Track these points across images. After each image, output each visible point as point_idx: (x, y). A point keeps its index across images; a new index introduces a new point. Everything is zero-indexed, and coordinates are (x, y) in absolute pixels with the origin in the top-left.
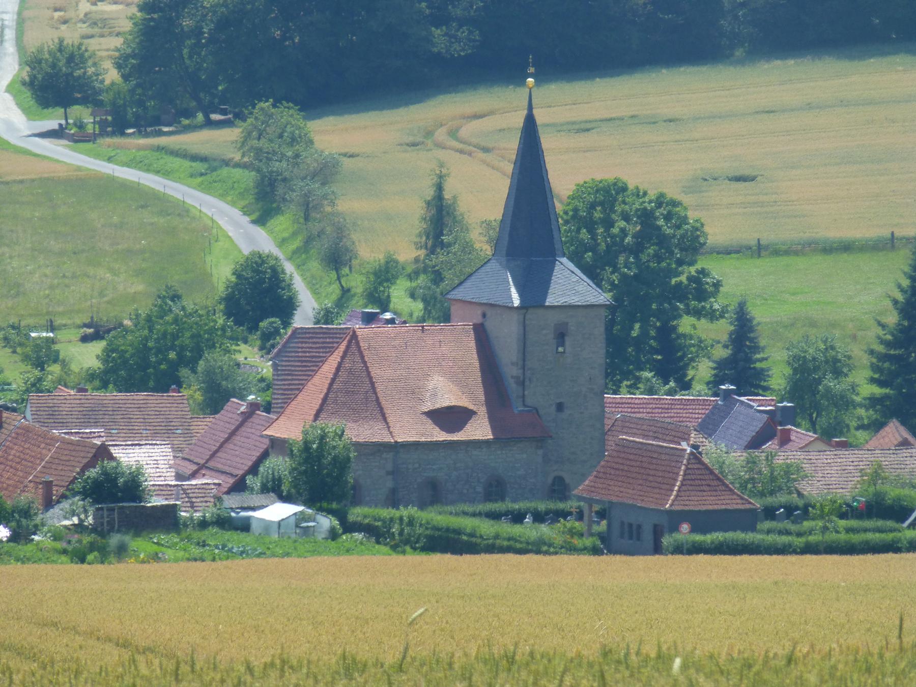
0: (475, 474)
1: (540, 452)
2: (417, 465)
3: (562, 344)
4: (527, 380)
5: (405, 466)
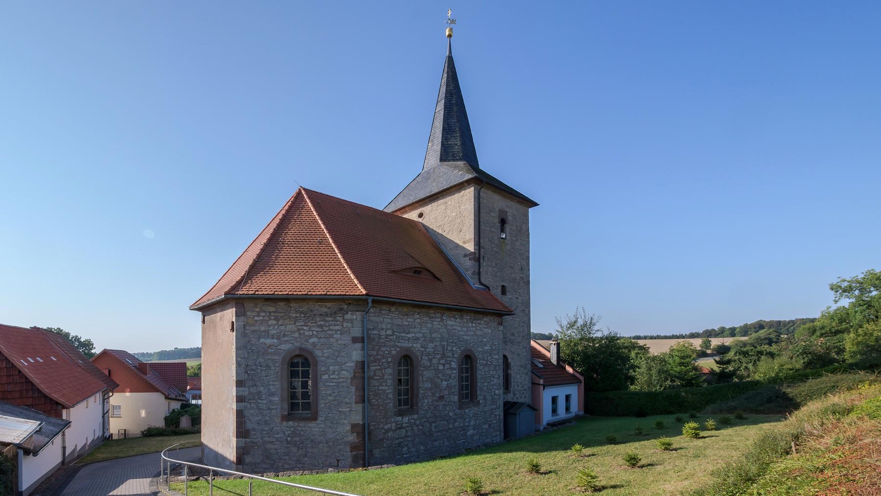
0: (449, 348)
1: (501, 328)
2: (389, 332)
3: (502, 231)
4: (481, 258)
5: (376, 332)
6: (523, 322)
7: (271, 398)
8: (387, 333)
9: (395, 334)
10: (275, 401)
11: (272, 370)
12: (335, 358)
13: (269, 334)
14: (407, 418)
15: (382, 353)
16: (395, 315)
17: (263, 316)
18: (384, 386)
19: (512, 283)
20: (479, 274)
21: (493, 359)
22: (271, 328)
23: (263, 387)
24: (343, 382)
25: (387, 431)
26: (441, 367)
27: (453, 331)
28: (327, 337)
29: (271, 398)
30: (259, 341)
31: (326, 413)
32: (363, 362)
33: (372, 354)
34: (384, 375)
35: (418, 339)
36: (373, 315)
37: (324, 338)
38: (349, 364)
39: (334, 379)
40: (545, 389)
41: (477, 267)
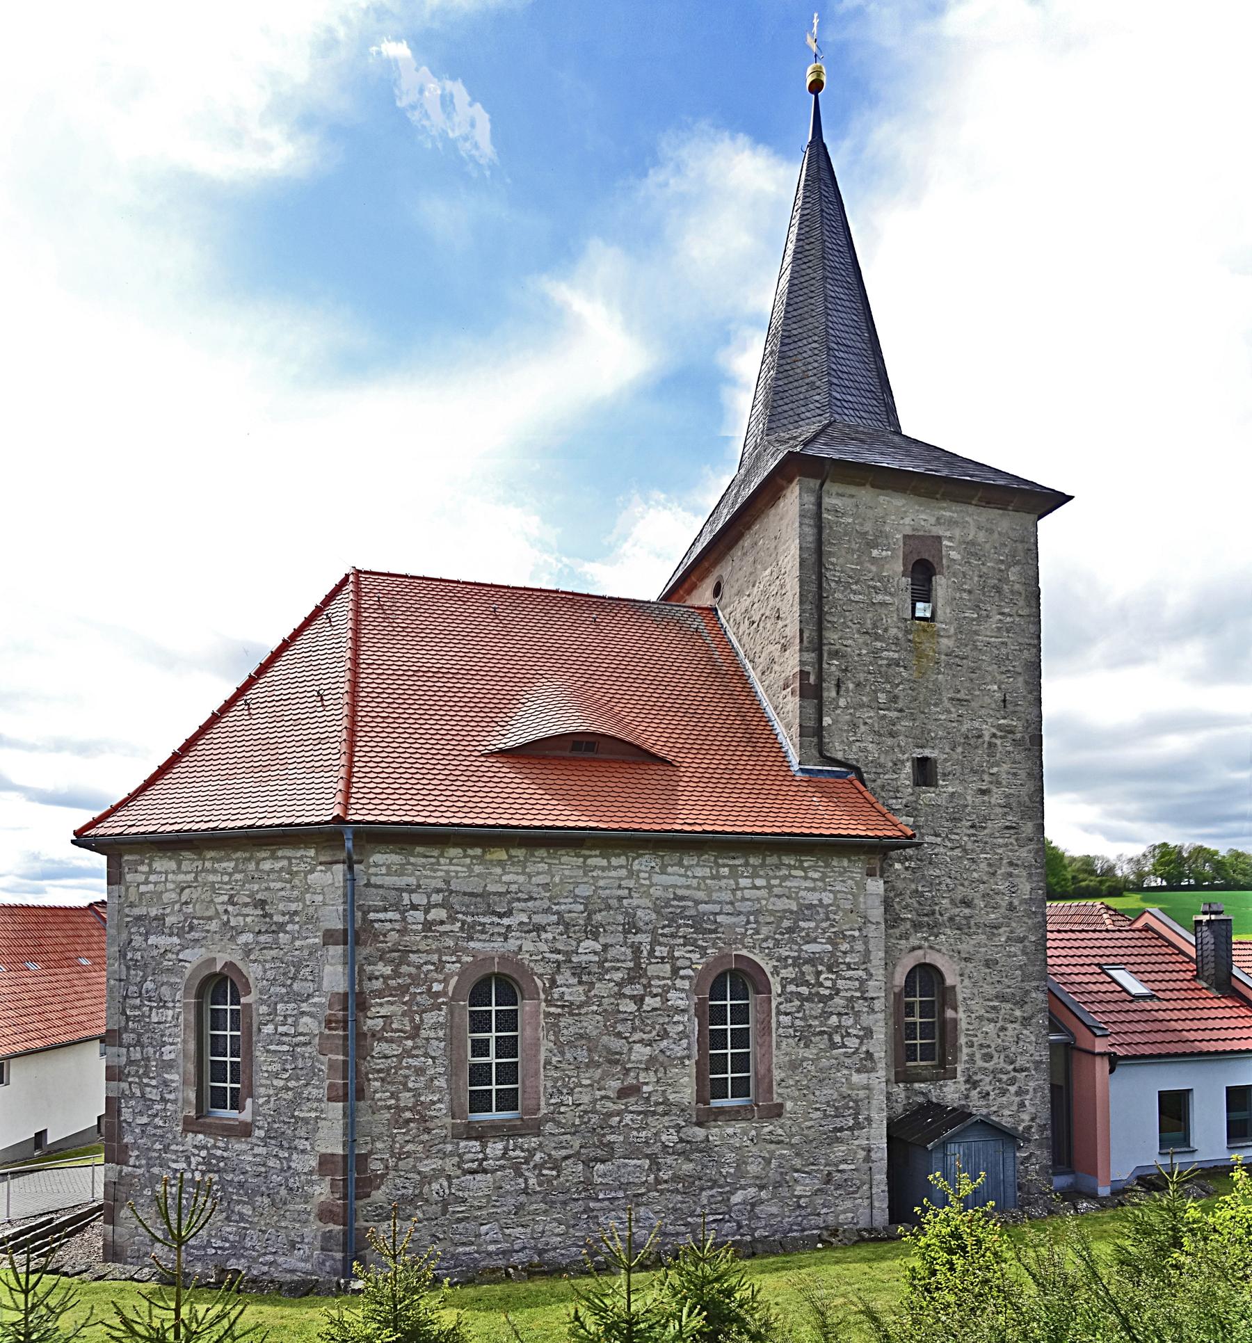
6: (1011, 864)
7: (165, 1076)
8: (429, 917)
9: (457, 920)
10: (173, 1081)
11: (168, 1008)
12: (289, 982)
13: (164, 924)
14: (500, 1146)
15: (413, 970)
16: (459, 868)
17: (155, 884)
18: (417, 1056)
19: (959, 750)
20: (819, 731)
21: (839, 982)
22: (168, 911)
23: (154, 1047)
24: (305, 1044)
25: (426, 1179)
26: (629, 1007)
27: (675, 903)
28: (273, 931)
29: (165, 1076)
30: (146, 940)
31: (269, 1120)
32: (346, 995)
33: (377, 973)
34: (417, 1028)
35: (539, 929)
36: (384, 871)
37: (267, 932)
38: (316, 1000)
39: (286, 1034)
40: (1118, 1070)
41: (811, 711)
